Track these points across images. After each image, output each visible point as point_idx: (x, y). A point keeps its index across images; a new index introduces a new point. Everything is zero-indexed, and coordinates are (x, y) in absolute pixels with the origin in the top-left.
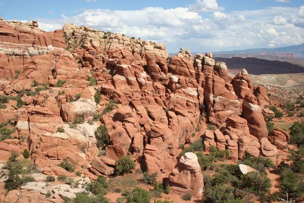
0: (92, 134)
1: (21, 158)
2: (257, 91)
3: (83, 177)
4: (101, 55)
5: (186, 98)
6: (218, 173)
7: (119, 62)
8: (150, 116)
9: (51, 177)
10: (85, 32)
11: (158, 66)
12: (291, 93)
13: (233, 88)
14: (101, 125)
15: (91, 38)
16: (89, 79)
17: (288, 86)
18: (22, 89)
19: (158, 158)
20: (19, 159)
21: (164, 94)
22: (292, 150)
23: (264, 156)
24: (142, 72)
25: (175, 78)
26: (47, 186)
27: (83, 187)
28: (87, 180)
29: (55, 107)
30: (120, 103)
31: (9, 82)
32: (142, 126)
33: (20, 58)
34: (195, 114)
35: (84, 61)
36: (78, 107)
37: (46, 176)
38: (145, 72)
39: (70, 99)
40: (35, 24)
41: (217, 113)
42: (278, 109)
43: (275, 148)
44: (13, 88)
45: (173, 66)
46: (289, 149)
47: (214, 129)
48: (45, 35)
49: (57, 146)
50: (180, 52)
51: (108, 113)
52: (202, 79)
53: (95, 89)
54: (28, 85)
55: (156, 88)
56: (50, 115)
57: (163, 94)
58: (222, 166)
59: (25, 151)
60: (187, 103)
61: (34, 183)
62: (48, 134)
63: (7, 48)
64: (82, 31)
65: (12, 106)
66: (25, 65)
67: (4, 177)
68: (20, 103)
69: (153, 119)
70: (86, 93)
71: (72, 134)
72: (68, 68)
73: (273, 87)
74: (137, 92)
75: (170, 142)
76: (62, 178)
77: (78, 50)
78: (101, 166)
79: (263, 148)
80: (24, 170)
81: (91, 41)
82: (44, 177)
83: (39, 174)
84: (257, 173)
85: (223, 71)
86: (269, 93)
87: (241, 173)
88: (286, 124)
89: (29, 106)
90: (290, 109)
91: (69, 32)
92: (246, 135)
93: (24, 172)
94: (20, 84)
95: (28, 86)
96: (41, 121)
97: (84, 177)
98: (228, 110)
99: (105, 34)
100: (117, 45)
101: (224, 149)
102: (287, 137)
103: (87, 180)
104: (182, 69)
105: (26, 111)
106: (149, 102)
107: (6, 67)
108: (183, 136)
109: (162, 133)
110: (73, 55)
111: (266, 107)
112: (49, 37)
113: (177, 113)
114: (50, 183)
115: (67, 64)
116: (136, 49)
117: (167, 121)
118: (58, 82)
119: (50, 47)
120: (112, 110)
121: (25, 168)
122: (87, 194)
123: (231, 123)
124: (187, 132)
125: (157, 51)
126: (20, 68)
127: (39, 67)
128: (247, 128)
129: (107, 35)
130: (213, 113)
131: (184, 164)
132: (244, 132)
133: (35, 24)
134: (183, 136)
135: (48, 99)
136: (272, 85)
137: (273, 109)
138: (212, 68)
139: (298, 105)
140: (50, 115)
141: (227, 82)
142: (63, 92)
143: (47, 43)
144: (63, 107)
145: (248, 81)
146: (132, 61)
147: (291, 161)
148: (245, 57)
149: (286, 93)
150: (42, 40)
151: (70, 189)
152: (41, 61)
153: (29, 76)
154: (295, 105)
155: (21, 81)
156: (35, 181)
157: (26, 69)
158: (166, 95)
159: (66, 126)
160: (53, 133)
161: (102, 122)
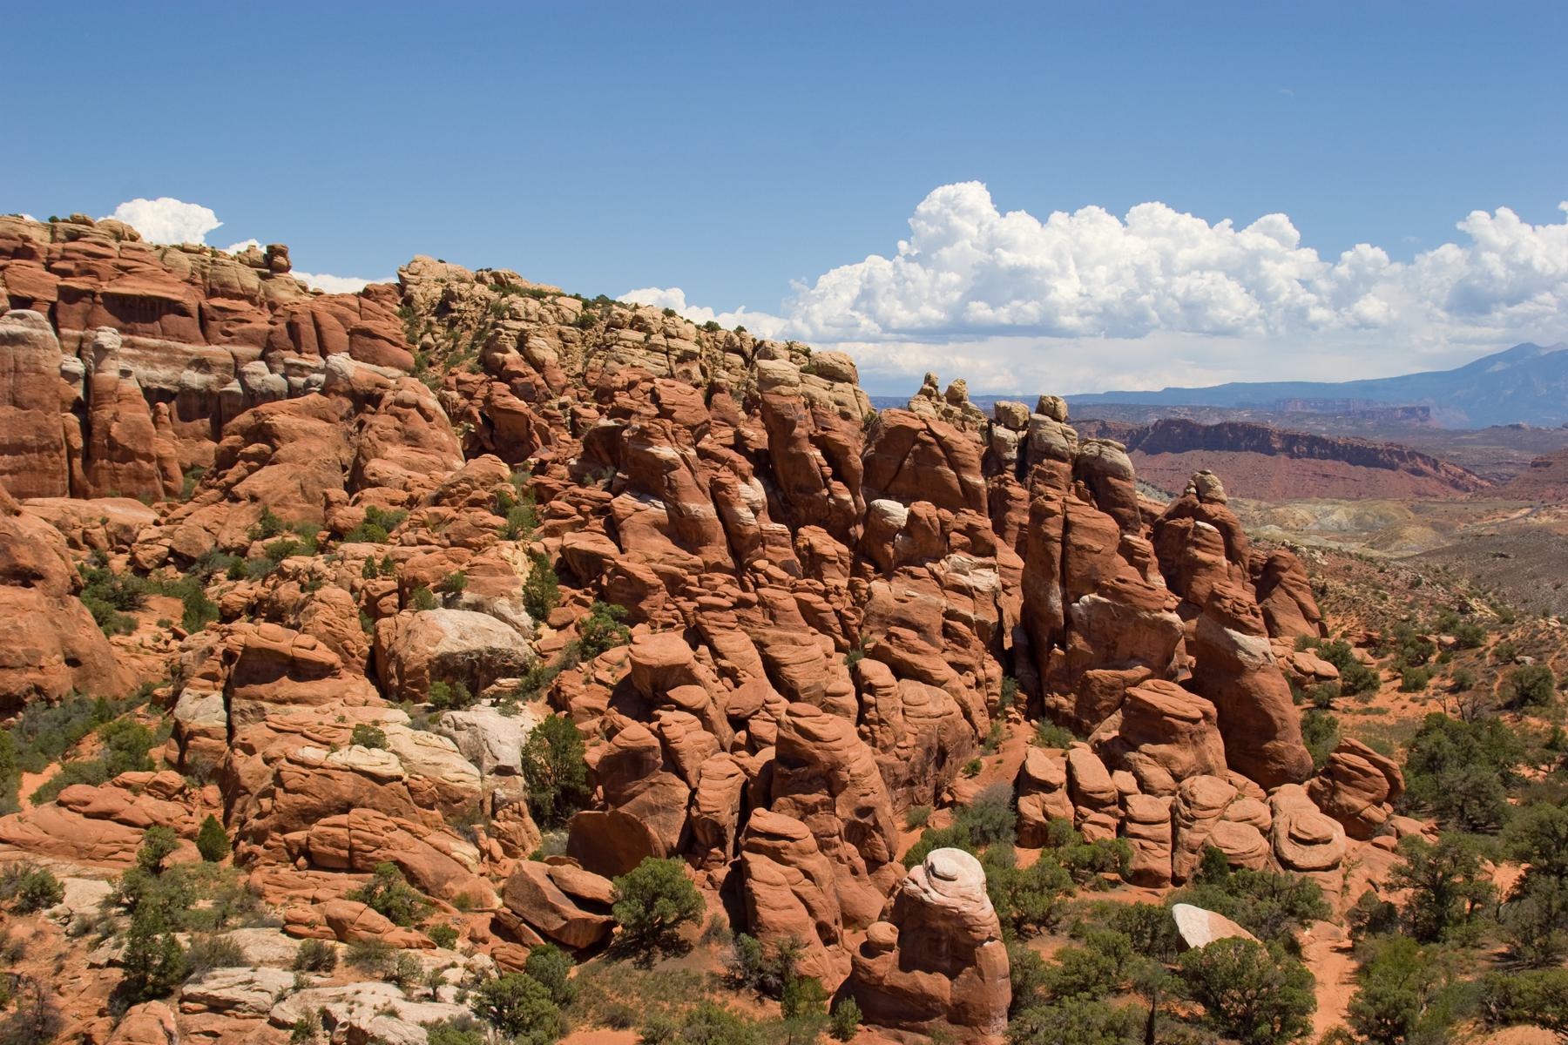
1: (187, 855)
2: (1266, 577)
3: (464, 952)
5: (944, 602)
6: (1077, 946)
7: (644, 436)
10: (494, 296)
11: (818, 453)
13: (1155, 559)
14: (550, 718)
15: (522, 325)
16: (501, 506)
17: (1405, 554)
18: (208, 545)
19: (807, 875)
20: (179, 861)
21: (843, 583)
22: (1413, 841)
23: (1287, 865)
25: (897, 511)
27: (460, 1000)
28: (482, 959)
31: (155, 516)
32: (738, 722)
34: (980, 673)
35: (495, 435)
36: (450, 631)
37: (298, 943)
38: (756, 482)
39: (410, 593)
40: (280, 260)
42: (1358, 653)
43: (1336, 830)
44: (168, 542)
45: (901, 457)
46: (1399, 836)
47: (1065, 746)
48: (319, 306)
49: (346, 808)
50: (922, 392)
51: (584, 665)
52: (1019, 517)
54: (236, 525)
55: (813, 563)
57: (837, 579)
58: (1102, 911)
59: (209, 824)
60: (945, 626)
61: (242, 973)
62: (312, 753)
63: (151, 364)
65: (161, 624)
66: (227, 441)
67: (112, 940)
68: (197, 612)
69: (791, 693)
70: (491, 570)
71: (417, 754)
72: (415, 457)
73: (1340, 554)
74: (718, 567)
75: (863, 801)
76: (369, 958)
77: (463, 376)
79: (1283, 835)
80: (198, 913)
81: (522, 341)
83: (266, 934)
84: (1251, 948)
86: (1319, 580)
87: (1182, 945)
88: (1389, 722)
89: (236, 625)
91: (427, 292)
92: (1208, 771)
93: (200, 923)
95: (233, 536)
97: (469, 954)
99: (586, 305)
100: (640, 357)
101: (1110, 836)
103: (482, 959)
105: (220, 649)
106: (772, 617)
110: (443, 401)
111: (1303, 644)
112: (337, 316)
113: (901, 670)
114: (314, 978)
115: (413, 440)
116: (724, 377)
117: (856, 704)
118: (368, 521)
119: (341, 360)
120: (603, 648)
121: (204, 905)
122: (478, 1029)
123: (1149, 726)
125: (817, 387)
126: (204, 453)
127: (285, 449)
128: (1215, 743)
131: (922, 903)
132: (1201, 757)
133: (280, 260)
136: (1334, 545)
137: (1337, 656)
138: (1066, 467)
139: (1445, 638)
141: (1135, 532)
142: (388, 564)
143: (329, 344)
144: (382, 631)
145: (1226, 530)
146: (698, 431)
148: (1216, 421)
149: (1397, 583)
150: (307, 329)
151: (401, 1006)
152: (295, 422)
153: (239, 489)
154: (1433, 638)
155: (205, 511)
156: (245, 964)
157: (226, 460)
158: (852, 587)
159: (394, 719)
160: (334, 748)
161: (558, 701)
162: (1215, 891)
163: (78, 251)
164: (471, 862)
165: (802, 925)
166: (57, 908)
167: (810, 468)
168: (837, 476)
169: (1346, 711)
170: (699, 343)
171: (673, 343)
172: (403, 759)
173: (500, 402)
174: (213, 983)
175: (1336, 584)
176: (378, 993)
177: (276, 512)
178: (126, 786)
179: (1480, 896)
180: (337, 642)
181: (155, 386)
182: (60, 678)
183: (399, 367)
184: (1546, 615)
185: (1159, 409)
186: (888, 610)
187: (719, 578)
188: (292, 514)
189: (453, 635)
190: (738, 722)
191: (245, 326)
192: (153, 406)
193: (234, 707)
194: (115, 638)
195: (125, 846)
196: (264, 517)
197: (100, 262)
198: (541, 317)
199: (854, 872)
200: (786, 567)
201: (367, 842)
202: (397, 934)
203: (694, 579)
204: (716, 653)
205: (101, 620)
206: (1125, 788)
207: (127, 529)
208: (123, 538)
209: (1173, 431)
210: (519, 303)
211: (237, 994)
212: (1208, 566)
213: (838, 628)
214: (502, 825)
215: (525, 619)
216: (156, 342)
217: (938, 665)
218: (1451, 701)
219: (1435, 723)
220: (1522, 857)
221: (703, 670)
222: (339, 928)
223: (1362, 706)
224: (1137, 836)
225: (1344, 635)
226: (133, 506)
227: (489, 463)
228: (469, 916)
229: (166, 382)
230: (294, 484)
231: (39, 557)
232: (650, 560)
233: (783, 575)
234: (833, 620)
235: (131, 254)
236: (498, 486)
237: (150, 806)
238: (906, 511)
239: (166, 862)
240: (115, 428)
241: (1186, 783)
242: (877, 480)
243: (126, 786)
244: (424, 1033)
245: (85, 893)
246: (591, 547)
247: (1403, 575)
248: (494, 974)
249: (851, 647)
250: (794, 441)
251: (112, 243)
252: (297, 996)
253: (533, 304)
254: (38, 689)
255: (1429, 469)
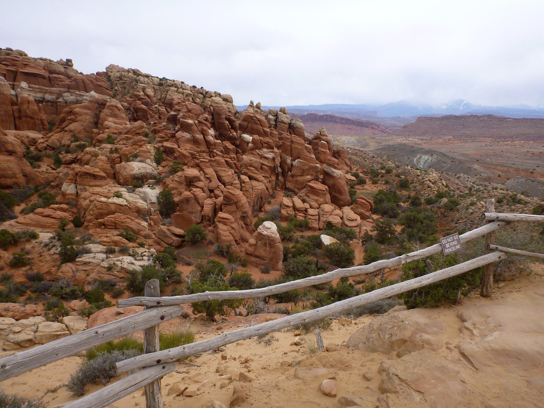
0: (154, 200)
1: (71, 226)
4: (156, 106)
5: (261, 161)
8: (220, 181)
9: (111, 249)
12: (374, 157)
15: (143, 85)
16: (146, 135)
18: (58, 144)
19: (232, 228)
23: (347, 226)
24: (209, 129)
25: (248, 137)
26: (107, 258)
29: (108, 168)
30: (185, 164)
33: (52, 106)
35: (136, 114)
36: (136, 167)
37: (105, 247)
38: (212, 129)
41: (295, 179)
53: (155, 147)
54: (66, 140)
56: (102, 178)
60: (261, 167)
61: (92, 255)
62: (103, 199)
63: (36, 92)
64: (131, 74)
65: (48, 166)
68: (58, 163)
69: (224, 184)
70: (145, 152)
72: (117, 121)
73: (354, 149)
74: (204, 152)
76: (124, 251)
77: (128, 99)
78: (167, 236)
81: (144, 90)
82: (101, 248)
83: (96, 245)
85: (299, 130)
90: (374, 176)
92: (326, 203)
93: (78, 243)
94: (55, 137)
96: (91, 184)
98: (308, 175)
102: (371, 206)
103: (153, 250)
104: (255, 126)
106: (219, 164)
107: (36, 117)
108: (257, 203)
109: (235, 200)
110: (122, 105)
111: (347, 173)
115: (115, 116)
119: (93, 93)
120: (176, 172)
121: (77, 238)
124: (262, 199)
128: (328, 197)
129: (164, 82)
130: (290, 179)
132: (325, 200)
133: (70, 63)
134: (257, 203)
135: (98, 158)
138: (287, 126)
140: (102, 178)
145: (328, 142)
147: (376, 232)
148: (322, 114)
155: (57, 134)
156: (92, 253)
159: (123, 190)
160: (109, 198)
161: (165, 185)
162: (329, 231)
163: (9, 59)
164: (146, 226)
165: (232, 240)
166: (37, 240)
167: (225, 126)
168: (232, 128)
169: (358, 189)
170: (191, 91)
171: (185, 91)
172: (127, 201)
173: (139, 106)
174: (84, 258)
175: (354, 157)
176: (127, 259)
177: (78, 135)
178: (52, 208)
179: (392, 232)
180: (104, 170)
181: (37, 99)
182: (22, 180)
183: (109, 96)
184: (408, 165)
185: (308, 110)
186: (248, 163)
187: (204, 154)
188: (82, 136)
189: (137, 169)
190: (211, 191)
191: (63, 83)
192: (38, 104)
193: (78, 187)
194: (35, 170)
195: (53, 224)
196: (74, 136)
197: (17, 62)
198: (148, 83)
199: (242, 228)
200: (221, 152)
201: (119, 221)
202: (131, 244)
203: (198, 154)
204: (205, 174)
205: (31, 164)
206: (307, 207)
207: (34, 139)
208: (34, 142)
209: (313, 117)
210: (142, 79)
211: (91, 260)
212: (325, 152)
213: (235, 167)
214: (153, 217)
215: (155, 164)
216: (37, 86)
217: (260, 177)
218: (384, 187)
219: (380, 192)
220: (402, 224)
221: (202, 178)
222: (116, 243)
223: (361, 188)
224: (310, 219)
225: (357, 170)
226: (35, 133)
227: (139, 123)
228: (147, 240)
229: (40, 98)
230: (82, 127)
231: (14, 147)
232: (186, 150)
233: (221, 154)
234: (234, 165)
235: (25, 60)
236: (143, 129)
237: (59, 213)
238: (251, 138)
239: (66, 228)
240: (28, 112)
241: (322, 206)
242: (245, 130)
243: (52, 208)
244: (141, 268)
245: (45, 236)
246: (171, 146)
247: (370, 155)
248: (156, 253)
249: (238, 173)
250: (221, 118)
251: (19, 56)
252: (107, 260)
253: (146, 79)
254: (16, 184)
255: (376, 128)
